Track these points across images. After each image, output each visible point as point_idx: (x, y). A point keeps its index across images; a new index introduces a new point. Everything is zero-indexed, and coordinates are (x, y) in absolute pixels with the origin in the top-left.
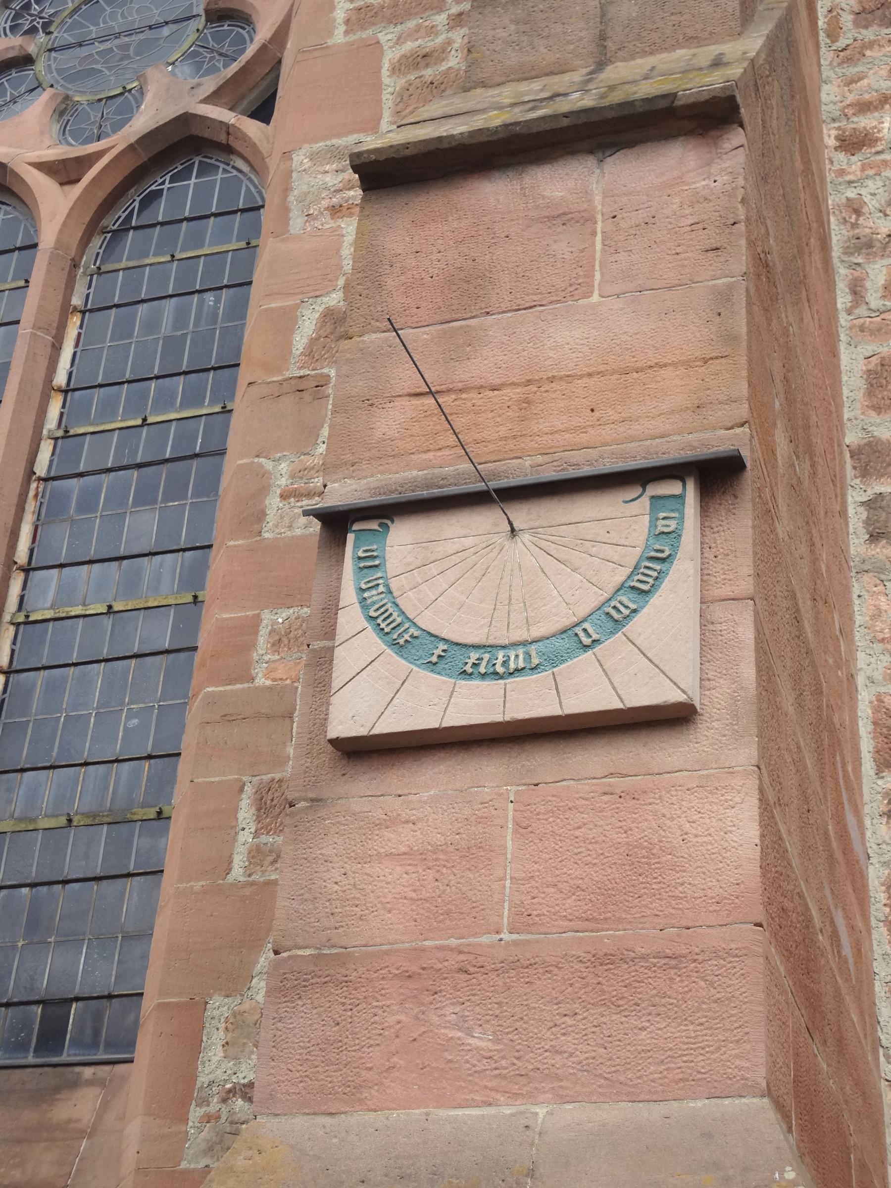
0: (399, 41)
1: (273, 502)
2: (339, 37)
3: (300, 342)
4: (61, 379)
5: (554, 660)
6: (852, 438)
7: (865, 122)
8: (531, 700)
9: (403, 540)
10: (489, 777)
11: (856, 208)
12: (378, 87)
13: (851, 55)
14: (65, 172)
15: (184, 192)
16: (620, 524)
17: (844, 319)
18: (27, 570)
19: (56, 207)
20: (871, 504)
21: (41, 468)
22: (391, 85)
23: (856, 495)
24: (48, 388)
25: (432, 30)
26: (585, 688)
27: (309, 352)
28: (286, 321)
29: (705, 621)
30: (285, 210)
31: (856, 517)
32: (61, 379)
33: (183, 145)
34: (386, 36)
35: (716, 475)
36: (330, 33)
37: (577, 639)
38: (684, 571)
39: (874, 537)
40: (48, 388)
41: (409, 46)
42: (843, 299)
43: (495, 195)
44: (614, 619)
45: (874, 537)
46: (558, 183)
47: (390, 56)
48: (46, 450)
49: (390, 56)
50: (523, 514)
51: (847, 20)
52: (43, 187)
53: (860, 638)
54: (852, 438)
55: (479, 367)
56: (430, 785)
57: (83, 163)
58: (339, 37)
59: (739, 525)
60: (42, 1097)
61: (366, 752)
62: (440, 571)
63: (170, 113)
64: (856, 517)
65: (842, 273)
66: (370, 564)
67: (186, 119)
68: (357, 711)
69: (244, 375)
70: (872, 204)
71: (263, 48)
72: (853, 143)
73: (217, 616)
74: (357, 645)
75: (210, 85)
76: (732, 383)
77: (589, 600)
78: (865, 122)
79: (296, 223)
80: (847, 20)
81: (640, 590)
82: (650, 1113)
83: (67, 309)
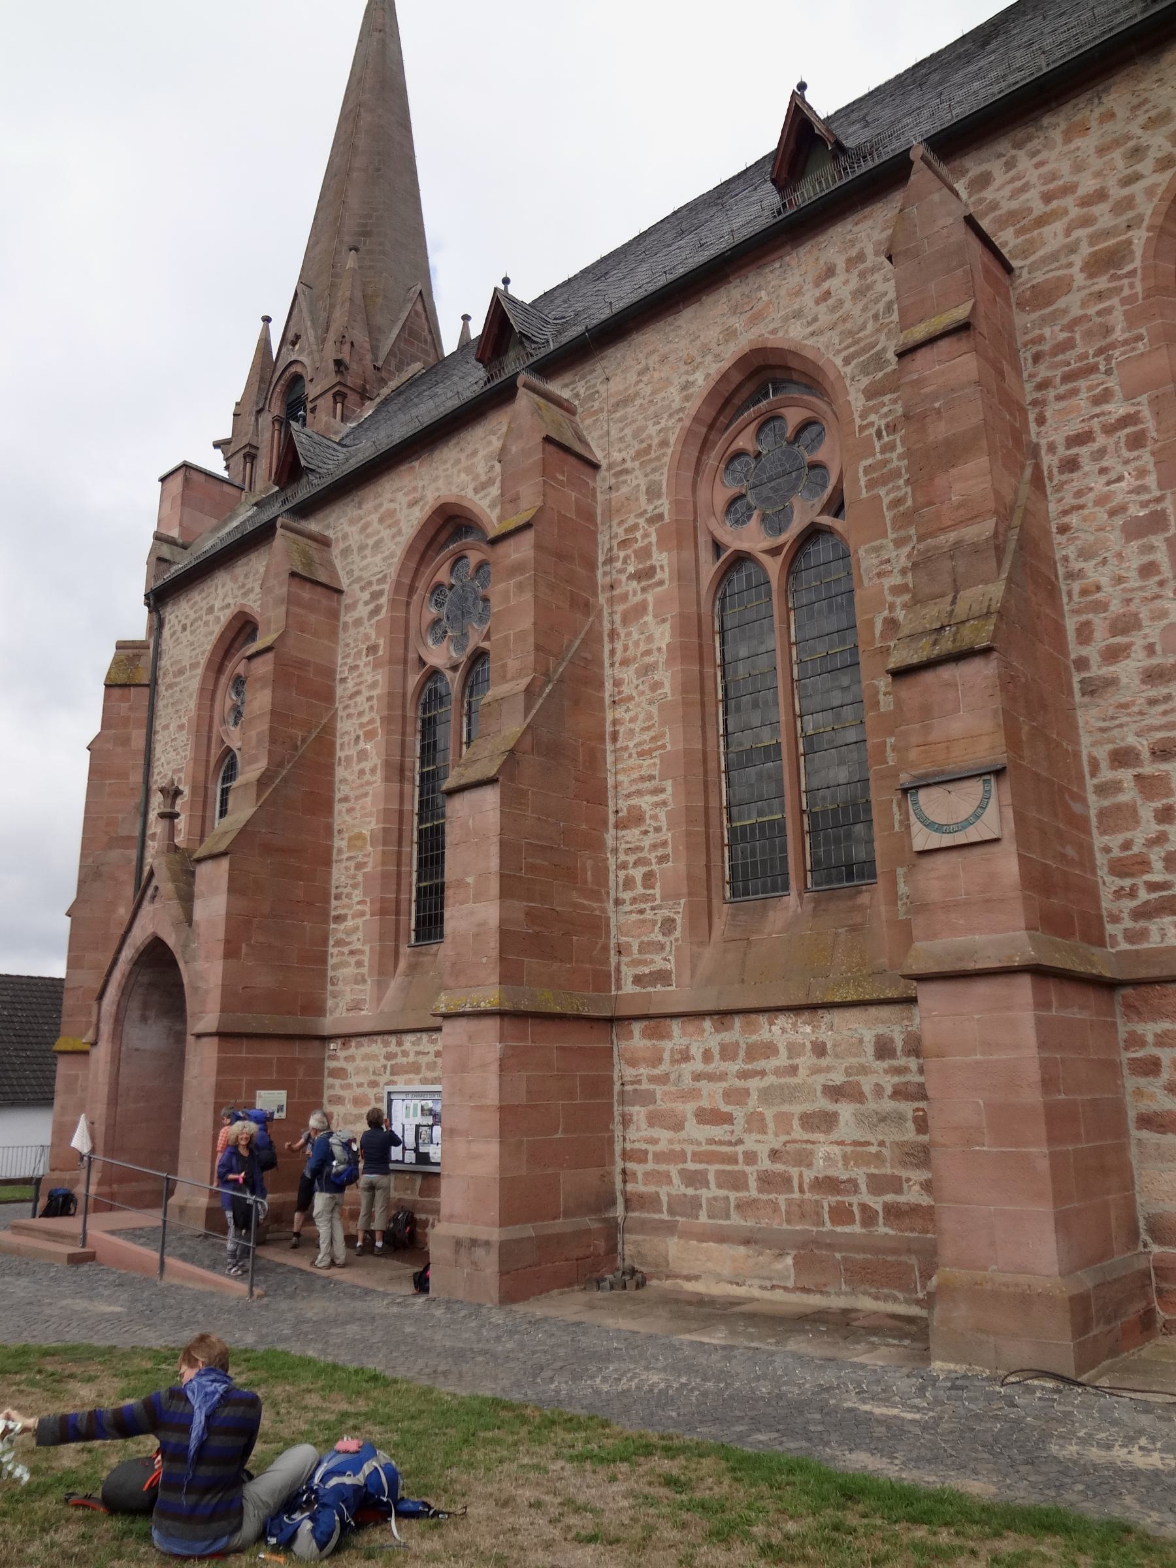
0: (888, 494)
1: (881, 697)
2: (864, 494)
3: (877, 632)
4: (793, 639)
5: (964, 828)
6: (1073, 656)
7: (1066, 520)
8: (960, 839)
9: (922, 794)
10: (953, 857)
11: (1066, 559)
12: (884, 517)
13: (1059, 488)
14: (774, 552)
15: (821, 550)
16: (975, 788)
17: (1066, 608)
18: (801, 716)
19: (774, 567)
20: (1082, 682)
21: (796, 677)
22: (888, 516)
23: (1076, 678)
24: (790, 644)
25: (899, 488)
26: (972, 835)
27: (882, 636)
28: (870, 624)
29: (1000, 812)
30: (860, 576)
31: (1076, 687)
32: (793, 639)
33: (813, 533)
34: (882, 491)
35: (999, 773)
36: (860, 492)
37: (968, 823)
38: (993, 802)
39: (1083, 694)
40: (790, 644)
41: (892, 496)
42: (1065, 599)
43: (928, 677)
44: (977, 816)
45: (1083, 694)
46: (946, 673)
47: (885, 502)
48: (795, 668)
49: (885, 502)
50: (950, 787)
51: (1055, 470)
52: (765, 559)
53: (1081, 732)
54: (1073, 656)
55: (934, 736)
56: (940, 859)
57: (781, 547)
58: (864, 494)
59: (1006, 786)
60: (852, 897)
61: (923, 853)
62: (931, 801)
63: (806, 522)
64: (1076, 687)
65: (1064, 588)
66: (916, 803)
67: (813, 524)
68: (919, 844)
69: (860, 650)
70: (1072, 556)
71: (835, 488)
72: (1063, 529)
73: (872, 741)
74: (916, 826)
75: (818, 509)
76: (1000, 739)
77: (971, 810)
78: (1066, 520)
79: (866, 581)
80: (1055, 470)
81: (982, 807)
82: (1000, 936)
83: (788, 610)
